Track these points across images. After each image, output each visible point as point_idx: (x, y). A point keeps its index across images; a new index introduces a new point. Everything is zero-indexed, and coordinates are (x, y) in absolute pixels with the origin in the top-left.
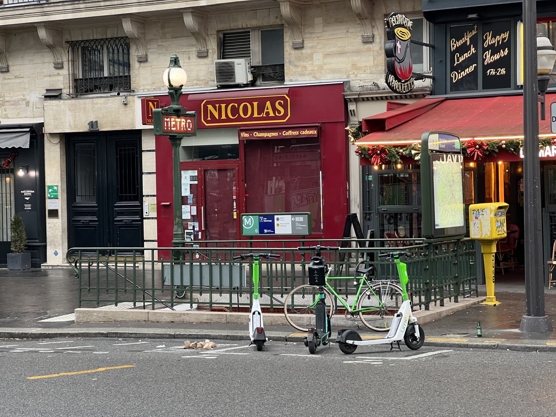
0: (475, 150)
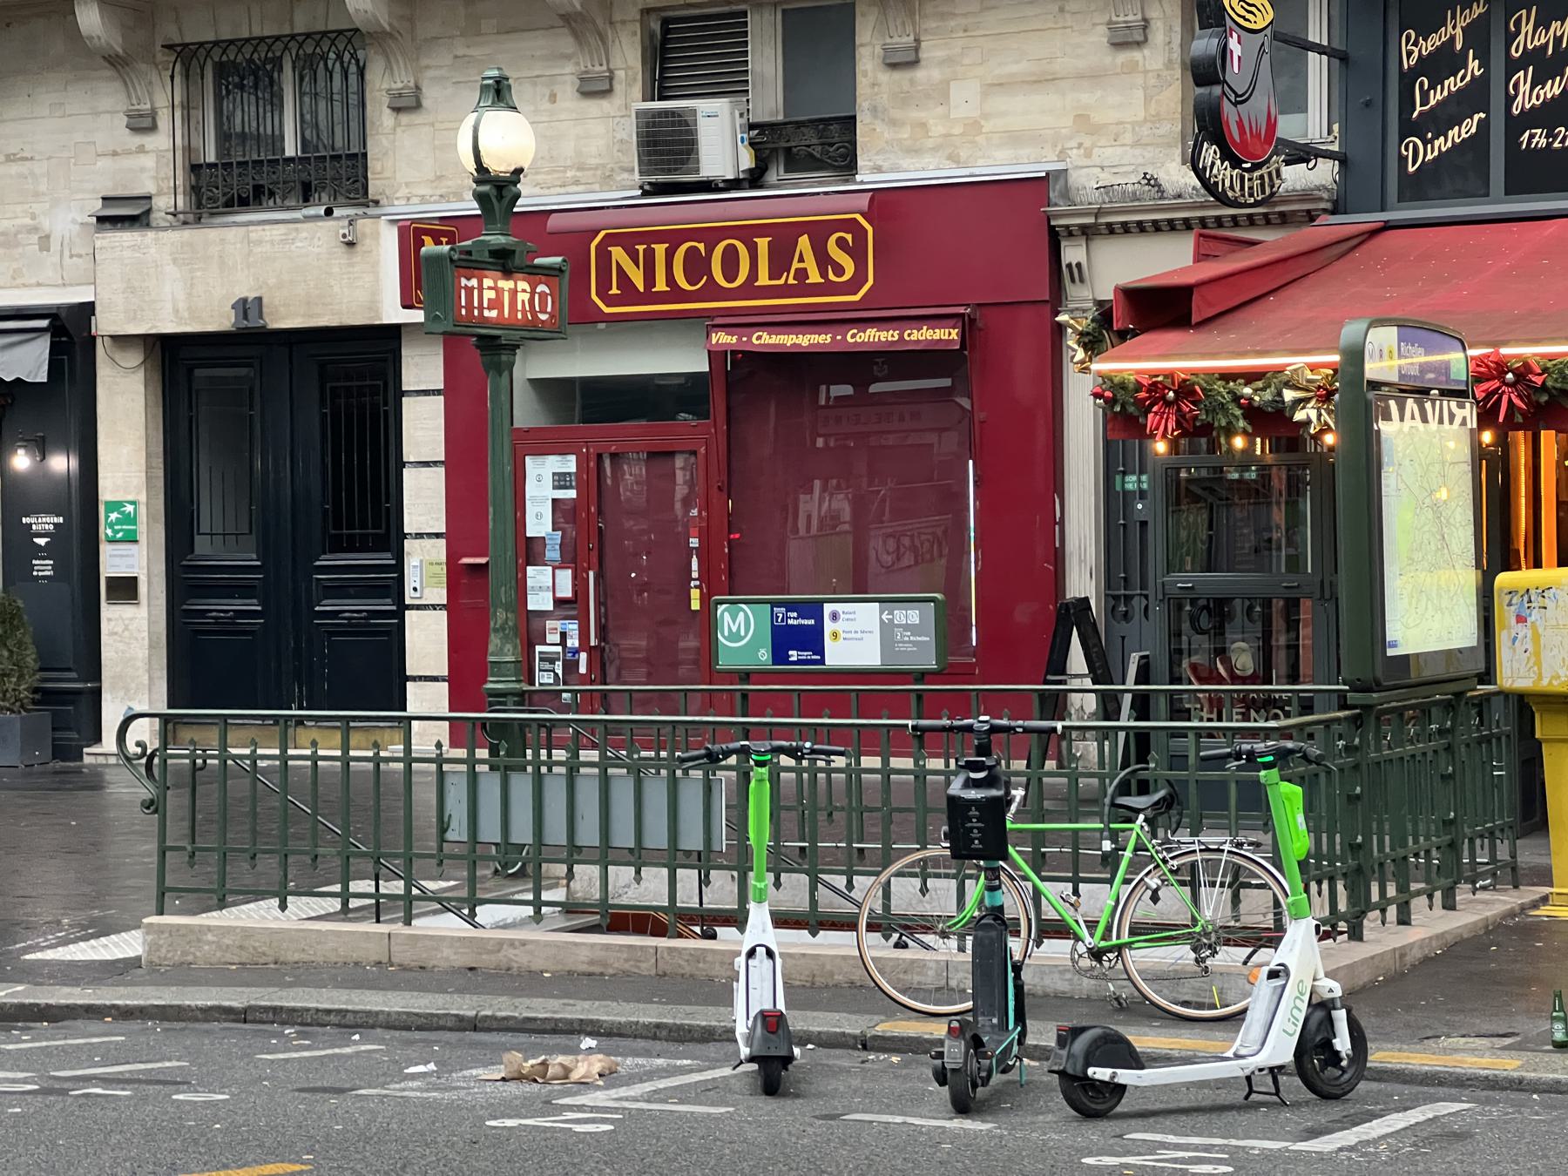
0: (1499, 388)
